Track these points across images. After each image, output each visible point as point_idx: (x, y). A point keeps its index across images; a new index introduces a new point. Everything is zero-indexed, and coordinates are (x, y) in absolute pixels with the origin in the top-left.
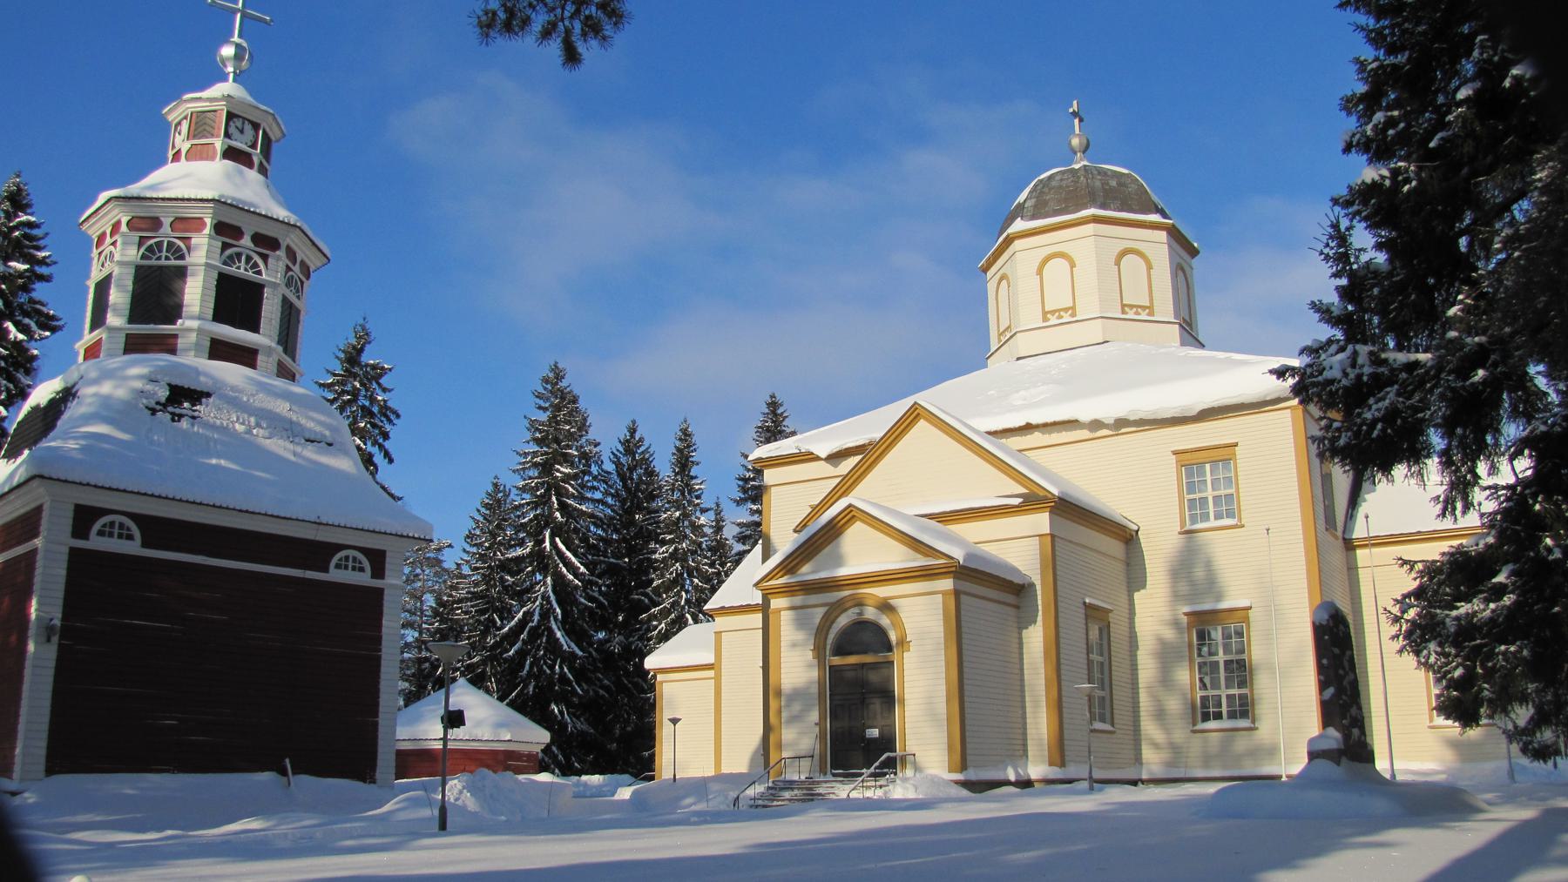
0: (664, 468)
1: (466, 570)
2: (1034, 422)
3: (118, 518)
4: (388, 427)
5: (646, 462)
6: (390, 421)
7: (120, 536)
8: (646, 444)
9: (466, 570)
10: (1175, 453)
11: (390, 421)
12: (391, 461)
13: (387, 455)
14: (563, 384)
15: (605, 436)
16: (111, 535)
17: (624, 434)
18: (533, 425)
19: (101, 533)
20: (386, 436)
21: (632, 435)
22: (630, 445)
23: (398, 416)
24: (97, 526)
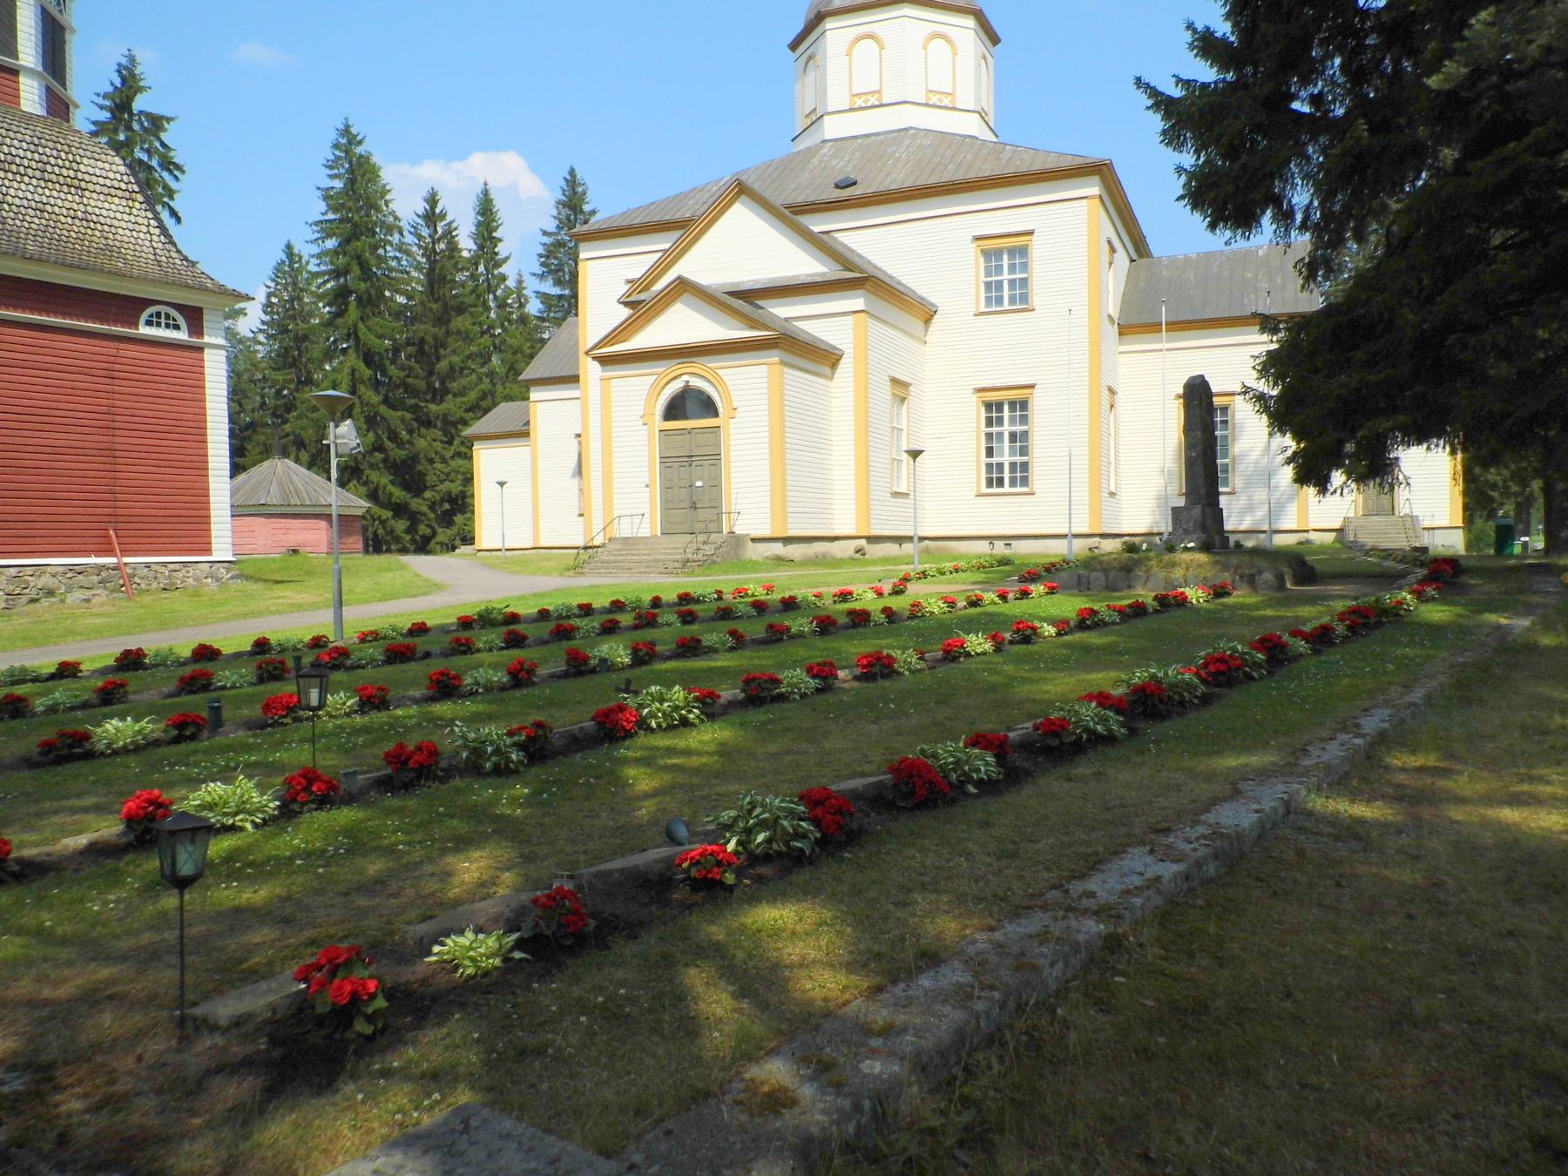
0: (466, 244)
1: (261, 338)
2: (780, 545)
3: (163, 309)
4: (173, 184)
5: (449, 234)
6: (177, 178)
7: (167, 326)
8: (449, 219)
9: (261, 338)
10: (978, 238)
11: (177, 178)
12: (178, 220)
13: (174, 214)
14: (359, 150)
15: (405, 205)
16: (159, 325)
17: (421, 207)
18: (327, 195)
19: (149, 323)
20: (171, 193)
21: (433, 208)
22: (431, 216)
23: (183, 172)
24: (144, 316)
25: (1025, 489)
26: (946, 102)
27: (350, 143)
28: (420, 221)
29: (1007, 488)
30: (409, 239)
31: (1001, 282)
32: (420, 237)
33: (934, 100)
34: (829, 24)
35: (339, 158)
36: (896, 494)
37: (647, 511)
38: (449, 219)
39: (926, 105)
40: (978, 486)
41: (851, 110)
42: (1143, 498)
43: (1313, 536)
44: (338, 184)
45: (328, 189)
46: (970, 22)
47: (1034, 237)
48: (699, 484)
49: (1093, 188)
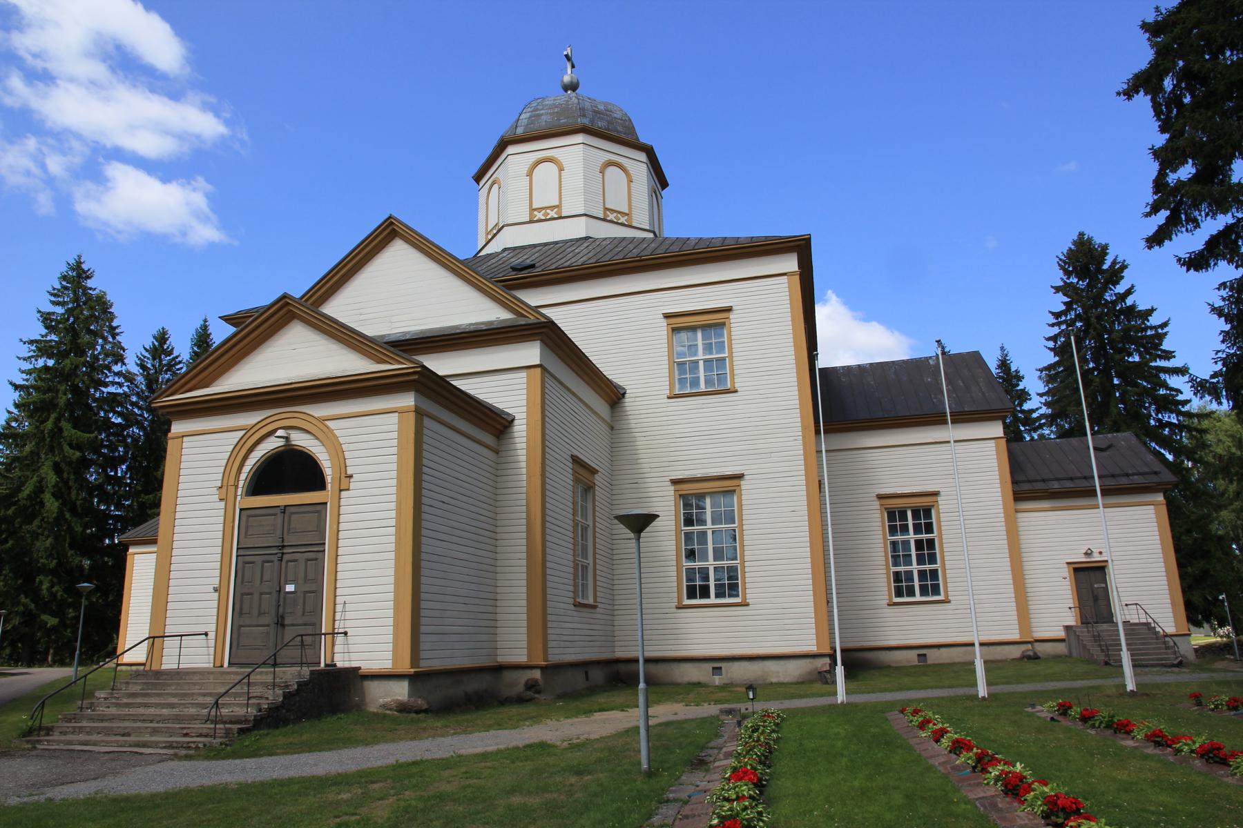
8: (175, 354)
17: (149, 342)
18: (46, 318)
25: (738, 600)
26: (623, 220)
27: (79, 276)
28: (147, 354)
29: (713, 600)
30: (135, 370)
31: (697, 362)
32: (143, 367)
33: (611, 217)
34: (511, 150)
35: (66, 288)
36: (578, 605)
37: (211, 628)
38: (175, 354)
39: (604, 220)
40: (890, 598)
41: (531, 222)
42: (1056, 613)
43: (1040, 648)
44: (60, 310)
45: (49, 314)
46: (642, 157)
47: (732, 316)
48: (290, 588)
49: (790, 263)
